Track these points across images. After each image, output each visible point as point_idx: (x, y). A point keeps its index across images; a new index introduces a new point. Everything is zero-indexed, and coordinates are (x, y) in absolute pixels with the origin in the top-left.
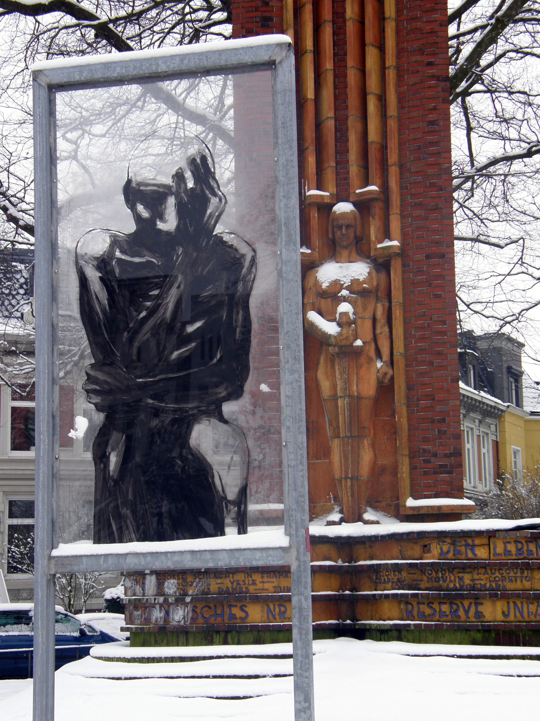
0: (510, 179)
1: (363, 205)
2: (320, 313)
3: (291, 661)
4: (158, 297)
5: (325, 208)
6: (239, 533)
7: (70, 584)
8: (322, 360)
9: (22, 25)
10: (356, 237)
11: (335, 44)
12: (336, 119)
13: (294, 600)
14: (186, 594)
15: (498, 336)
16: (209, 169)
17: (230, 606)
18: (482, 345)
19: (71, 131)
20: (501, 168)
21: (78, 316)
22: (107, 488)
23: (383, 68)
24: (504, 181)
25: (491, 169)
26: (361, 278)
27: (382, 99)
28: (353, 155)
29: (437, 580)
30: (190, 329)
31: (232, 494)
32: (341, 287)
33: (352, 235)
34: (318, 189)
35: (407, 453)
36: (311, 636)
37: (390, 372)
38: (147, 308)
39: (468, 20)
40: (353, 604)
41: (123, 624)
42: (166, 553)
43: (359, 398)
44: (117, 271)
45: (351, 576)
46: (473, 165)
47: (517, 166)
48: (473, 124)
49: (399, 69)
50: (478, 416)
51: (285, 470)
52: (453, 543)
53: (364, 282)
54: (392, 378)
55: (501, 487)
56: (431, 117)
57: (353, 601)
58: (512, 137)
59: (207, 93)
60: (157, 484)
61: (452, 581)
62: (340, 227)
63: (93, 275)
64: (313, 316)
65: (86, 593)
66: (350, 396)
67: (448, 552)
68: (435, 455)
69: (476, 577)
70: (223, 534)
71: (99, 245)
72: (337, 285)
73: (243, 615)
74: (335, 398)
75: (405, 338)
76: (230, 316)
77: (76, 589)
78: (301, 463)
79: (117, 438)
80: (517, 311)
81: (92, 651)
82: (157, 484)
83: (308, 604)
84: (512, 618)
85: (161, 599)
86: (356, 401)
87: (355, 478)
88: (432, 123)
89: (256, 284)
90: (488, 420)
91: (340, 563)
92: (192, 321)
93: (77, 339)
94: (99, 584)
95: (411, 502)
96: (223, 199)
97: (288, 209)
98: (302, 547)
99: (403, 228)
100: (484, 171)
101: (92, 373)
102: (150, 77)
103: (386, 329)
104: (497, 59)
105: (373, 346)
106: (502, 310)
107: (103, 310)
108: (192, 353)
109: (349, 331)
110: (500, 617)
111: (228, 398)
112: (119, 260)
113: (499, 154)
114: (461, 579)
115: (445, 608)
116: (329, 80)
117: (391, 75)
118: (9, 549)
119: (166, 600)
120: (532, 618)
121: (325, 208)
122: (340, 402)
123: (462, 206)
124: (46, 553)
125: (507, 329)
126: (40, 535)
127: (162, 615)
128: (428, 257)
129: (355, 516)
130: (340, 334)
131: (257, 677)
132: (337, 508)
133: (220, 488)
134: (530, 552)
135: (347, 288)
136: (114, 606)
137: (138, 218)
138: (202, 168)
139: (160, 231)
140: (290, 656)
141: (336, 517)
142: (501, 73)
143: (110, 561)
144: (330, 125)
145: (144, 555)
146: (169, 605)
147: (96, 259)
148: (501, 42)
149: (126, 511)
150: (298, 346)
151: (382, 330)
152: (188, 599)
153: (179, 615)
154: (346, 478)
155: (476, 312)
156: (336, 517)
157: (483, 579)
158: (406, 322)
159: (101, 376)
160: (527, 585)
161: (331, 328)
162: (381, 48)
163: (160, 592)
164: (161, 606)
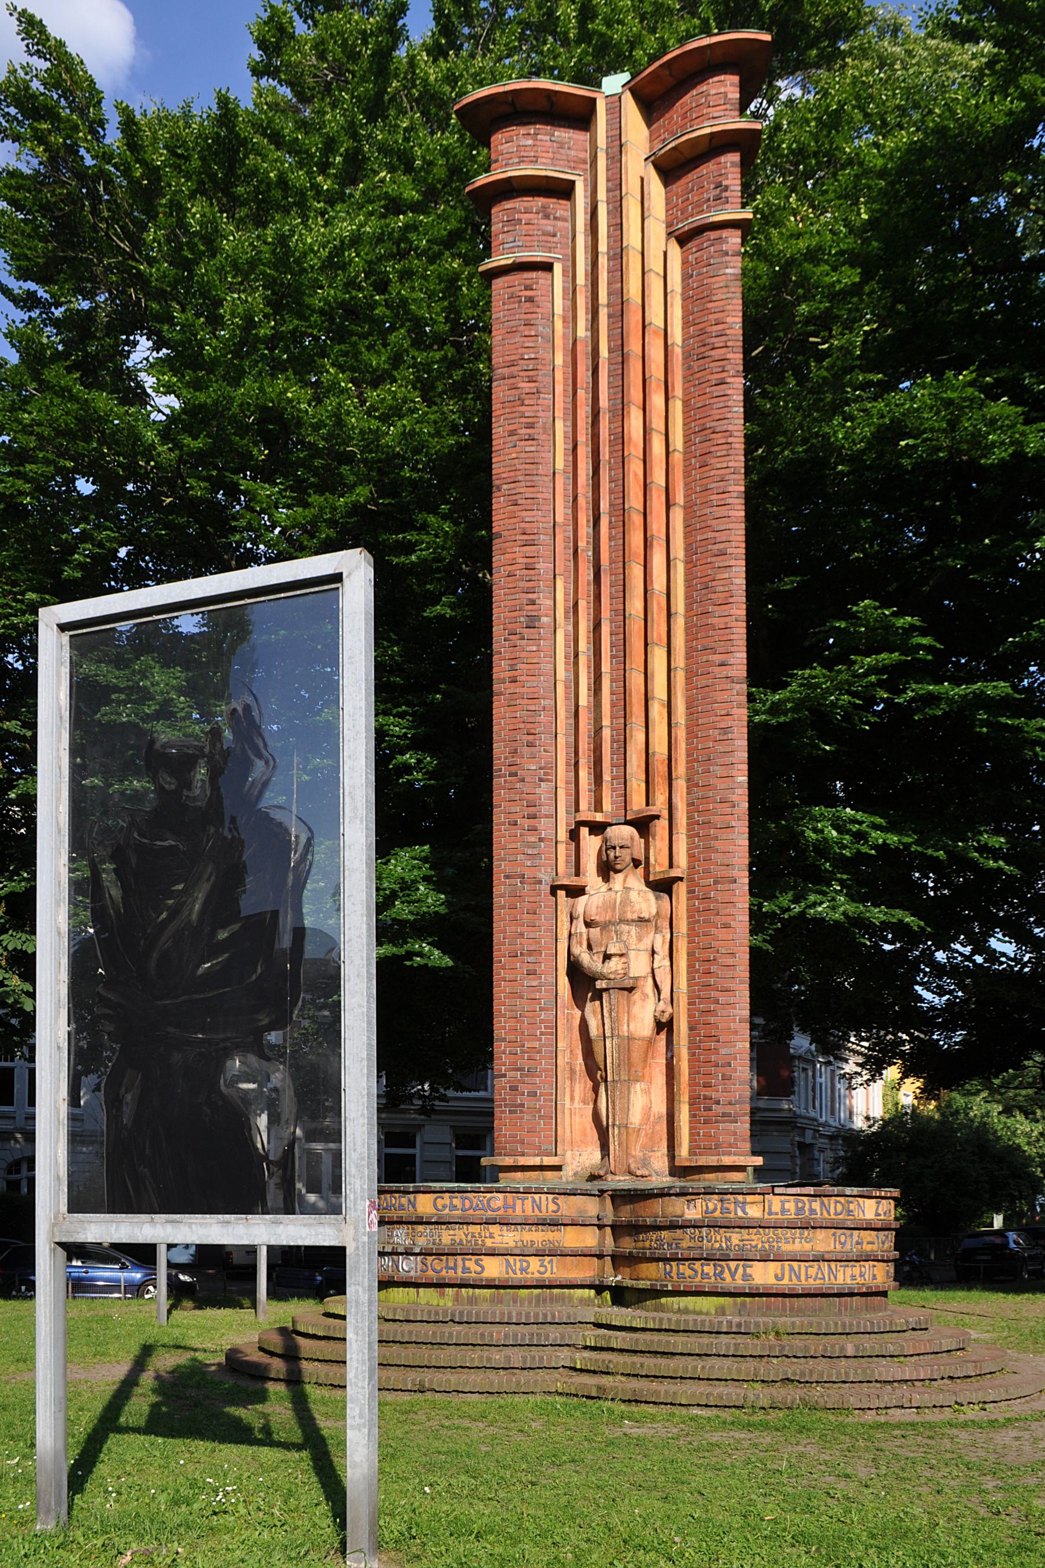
16: (254, 721)
37: (670, 1010)
38: (168, 908)
43: (630, 1039)
62: (614, 848)
67: (715, 1209)
69: (747, 1237)
84: (786, 1281)
114: (728, 1239)
120: (811, 1281)
134: (812, 1211)
157: (756, 1240)
158: (690, 954)
160: (807, 1246)
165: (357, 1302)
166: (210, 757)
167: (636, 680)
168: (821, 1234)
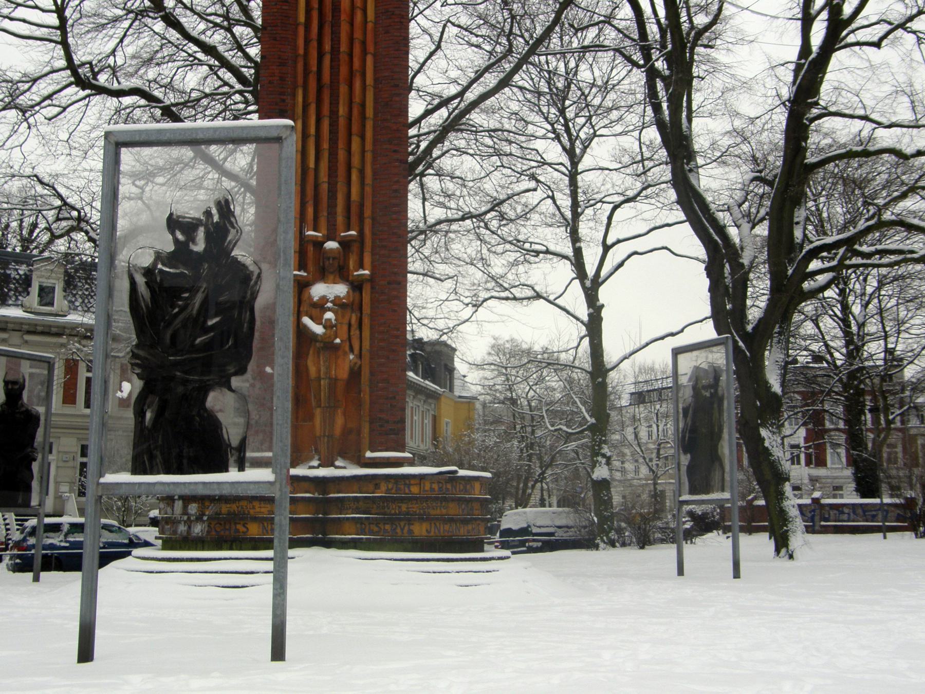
0: (450, 235)
1: (345, 244)
2: (312, 318)
3: (272, 562)
4: (187, 298)
5: (318, 244)
6: (239, 471)
7: (124, 506)
8: (311, 352)
9: (108, 105)
10: (339, 266)
11: (331, 132)
12: (329, 183)
13: (277, 519)
14: (204, 514)
15: (437, 343)
17: (236, 524)
18: (428, 349)
19: (139, 179)
20: (444, 227)
21: (128, 310)
22: (142, 435)
23: (363, 152)
24: (445, 236)
25: (438, 227)
26: (342, 295)
27: (362, 172)
28: (340, 209)
29: (384, 508)
30: (210, 323)
31: (235, 442)
32: (327, 301)
33: (336, 265)
34: (315, 230)
35: (368, 419)
36: (287, 544)
37: (359, 363)
38: (179, 306)
39: (425, 126)
40: (324, 522)
41: (157, 534)
42: (184, 484)
43: (336, 379)
44: (158, 279)
45: (325, 504)
46: (425, 223)
47: (454, 227)
48: (427, 196)
49: (374, 152)
50: (423, 398)
51: (275, 427)
52: (396, 483)
53: (344, 298)
54: (360, 367)
55: (436, 447)
56: (395, 187)
57: (324, 522)
58: (452, 206)
59: (242, 159)
60: (178, 433)
61: (393, 509)
63: (140, 280)
64: (306, 320)
65: (136, 512)
66: (330, 378)
68: (387, 422)
70: (227, 471)
71: (146, 260)
72: (324, 299)
73: (245, 530)
74: (319, 379)
75: (371, 339)
76: (240, 314)
77: (128, 510)
78: (287, 423)
79: (155, 400)
80: (451, 325)
81: (133, 553)
82: (178, 433)
83: (286, 522)
84: (432, 534)
85: (185, 518)
86: (334, 382)
87: (330, 436)
88: (396, 191)
89: (260, 294)
90: (430, 401)
91: (316, 495)
92: (212, 318)
93: (124, 323)
94: (146, 507)
95: (369, 454)
96: (240, 231)
97: (288, 241)
98: (284, 482)
99: (372, 262)
100: (432, 228)
101: (136, 351)
102: (195, 141)
103: (358, 332)
104: (443, 154)
105: (348, 343)
106: (441, 324)
107: (147, 306)
108: (212, 338)
109: (331, 332)
110: (424, 533)
111: (236, 374)
112: (161, 271)
113: (443, 217)
114: (400, 507)
115: (388, 527)
116: (325, 156)
117: (369, 156)
118: (80, 480)
119: (189, 518)
121: (318, 244)
122: (322, 382)
123: (417, 251)
124: (95, 480)
125: (445, 338)
126: (91, 469)
127: (186, 528)
128: (389, 283)
129: (327, 462)
130: (325, 334)
131: (252, 573)
132: (317, 457)
133: (226, 436)
134: (447, 489)
135: (331, 302)
136: (154, 522)
137: (176, 241)
138: (225, 207)
139: (192, 251)
140: (271, 559)
141: (315, 463)
142: (447, 163)
143: (143, 487)
144: (325, 187)
145: (168, 484)
146: (191, 521)
147: (144, 268)
148: (446, 143)
149: (157, 453)
150: (288, 338)
151: (355, 332)
152: (205, 518)
153: (198, 529)
154: (324, 436)
155: (424, 325)
156: (315, 463)
157: (415, 508)
158: (372, 328)
159: (141, 353)
160: (444, 511)
161: (318, 329)
162: (363, 137)
163: (185, 512)
164: (185, 522)
165: (281, 525)
166: (206, 226)
167: (342, 155)
168: (451, 505)
